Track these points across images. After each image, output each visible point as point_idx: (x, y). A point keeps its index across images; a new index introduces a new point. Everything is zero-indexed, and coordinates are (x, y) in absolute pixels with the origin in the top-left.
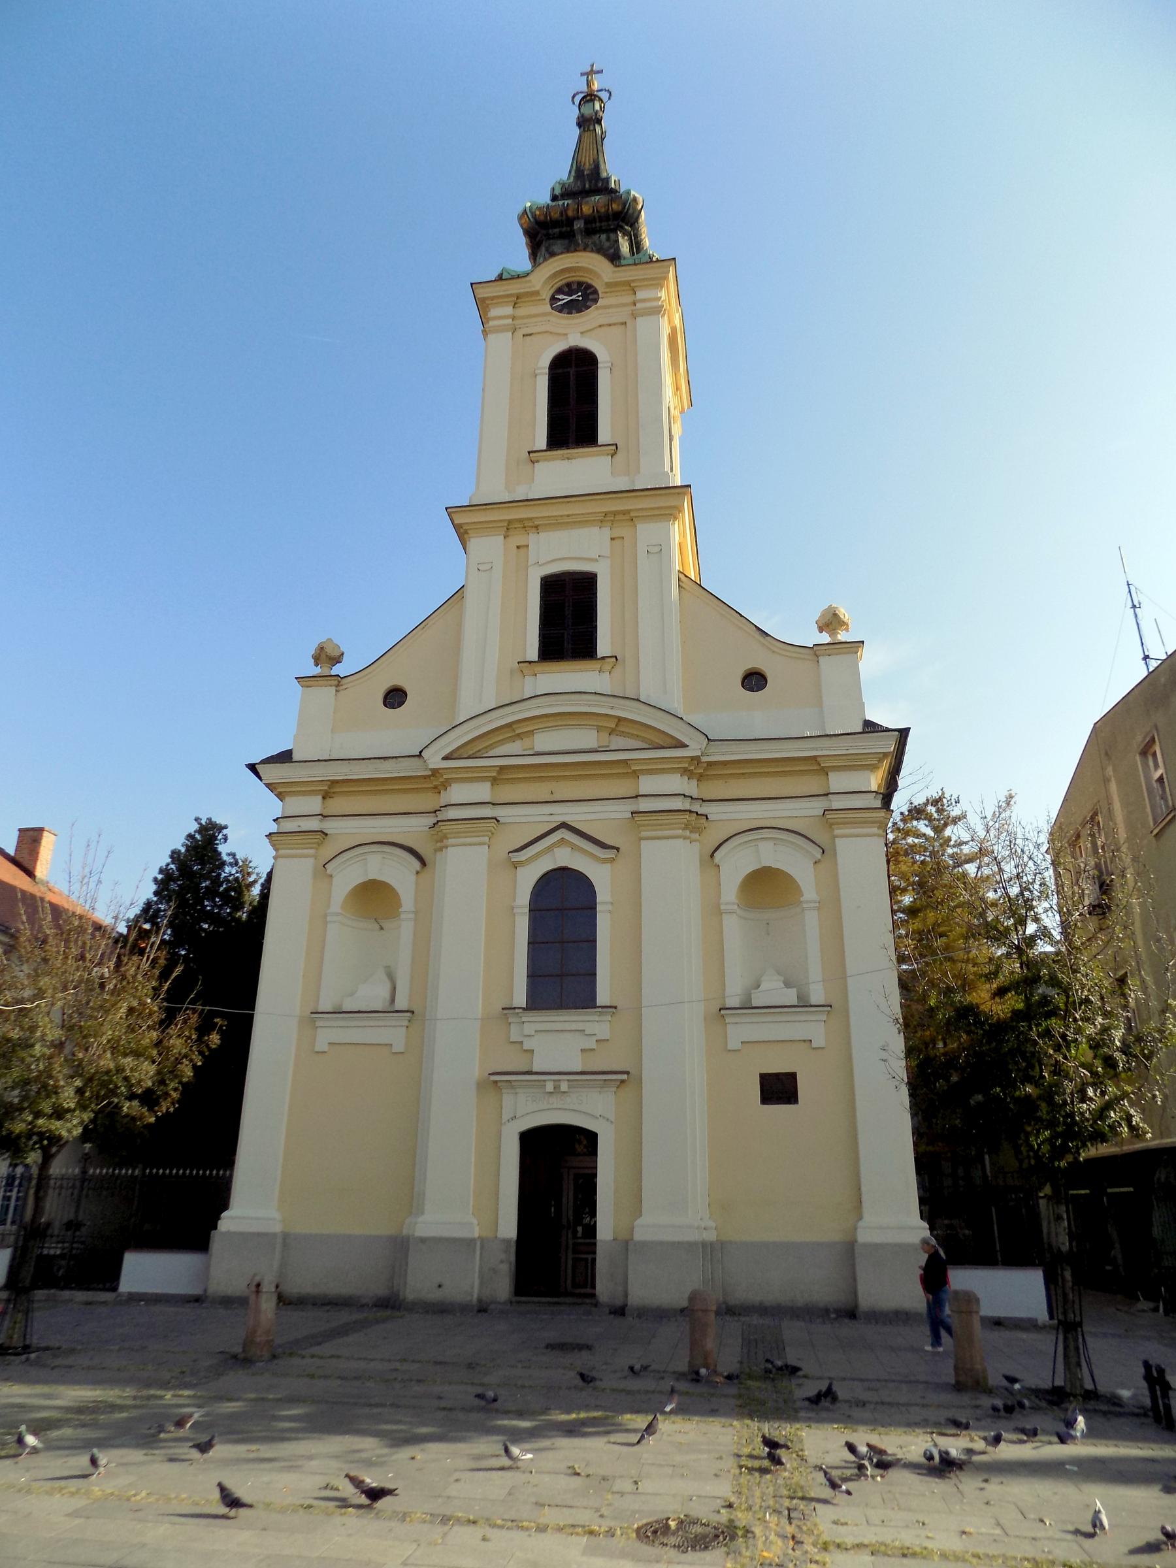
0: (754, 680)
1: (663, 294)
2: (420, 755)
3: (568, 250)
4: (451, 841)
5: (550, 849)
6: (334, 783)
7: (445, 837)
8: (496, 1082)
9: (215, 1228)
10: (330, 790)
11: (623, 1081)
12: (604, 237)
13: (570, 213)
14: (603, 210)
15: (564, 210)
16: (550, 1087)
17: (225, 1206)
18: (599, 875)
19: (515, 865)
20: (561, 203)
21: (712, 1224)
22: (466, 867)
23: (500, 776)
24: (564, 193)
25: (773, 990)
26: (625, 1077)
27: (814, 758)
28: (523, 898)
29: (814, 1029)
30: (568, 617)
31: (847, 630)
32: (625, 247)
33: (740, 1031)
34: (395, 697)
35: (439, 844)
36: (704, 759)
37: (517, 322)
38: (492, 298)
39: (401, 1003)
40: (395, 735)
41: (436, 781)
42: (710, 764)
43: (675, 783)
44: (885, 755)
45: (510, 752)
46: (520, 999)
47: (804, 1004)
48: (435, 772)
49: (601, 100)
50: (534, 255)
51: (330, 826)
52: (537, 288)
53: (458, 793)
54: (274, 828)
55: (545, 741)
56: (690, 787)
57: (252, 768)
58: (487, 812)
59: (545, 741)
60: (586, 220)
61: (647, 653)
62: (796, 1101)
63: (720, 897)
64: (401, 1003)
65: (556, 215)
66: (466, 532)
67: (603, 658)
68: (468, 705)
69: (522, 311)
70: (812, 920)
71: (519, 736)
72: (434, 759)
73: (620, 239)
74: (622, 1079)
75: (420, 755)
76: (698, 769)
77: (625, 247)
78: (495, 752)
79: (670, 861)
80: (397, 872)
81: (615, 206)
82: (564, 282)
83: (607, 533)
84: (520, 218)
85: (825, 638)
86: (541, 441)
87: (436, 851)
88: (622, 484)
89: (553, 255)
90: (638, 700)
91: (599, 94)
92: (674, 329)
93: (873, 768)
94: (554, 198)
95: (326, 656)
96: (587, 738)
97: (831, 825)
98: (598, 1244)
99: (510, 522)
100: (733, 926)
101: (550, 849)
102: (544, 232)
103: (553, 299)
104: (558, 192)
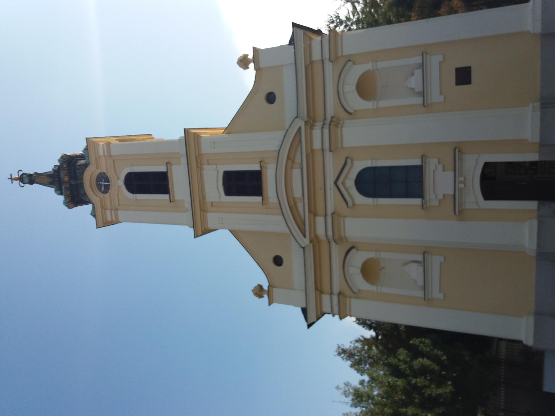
0: (271, 98)
1: (101, 143)
2: (304, 248)
3: (83, 187)
4: (342, 234)
5: (346, 189)
6: (316, 289)
7: (340, 237)
8: (459, 212)
9: (531, 348)
10: (319, 290)
11: (459, 151)
12: (78, 171)
13: (68, 186)
15: (67, 189)
16: (462, 186)
17: (520, 342)
18: (359, 165)
19: (354, 204)
21: (531, 105)
22: (355, 228)
23: (313, 213)
24: (60, 191)
25: (415, 82)
26: (457, 150)
27: (306, 67)
28: (369, 201)
29: (434, 61)
30: (243, 183)
31: (247, 55)
32: (82, 162)
33: (435, 97)
34: (278, 261)
35: (344, 240)
36: (306, 119)
39: (420, 258)
40: (295, 262)
41: (315, 241)
42: (308, 116)
43: (316, 133)
44: (304, 33)
45: (302, 208)
46: (417, 201)
47: (422, 66)
48: (311, 242)
49: (22, 174)
50: (86, 202)
51: (336, 290)
52: (98, 199)
53: (320, 231)
54: (337, 317)
55: (297, 192)
56: (319, 125)
57: (309, 326)
58: (329, 219)
59: (297, 192)
60: (70, 179)
61: (259, 150)
62: (469, 68)
63: (528, 33)
64: (420, 258)
65: (69, 192)
66: (205, 229)
67: (261, 167)
69: (109, 206)
70: (381, 65)
71: (295, 204)
72: (306, 242)
74: (458, 151)
75: (304, 248)
76: (310, 123)
77: (82, 162)
79: (353, 135)
80: (358, 259)
81: (65, 166)
83: (206, 167)
84: (70, 208)
85: (252, 66)
86: (165, 197)
88: (184, 160)
89: (85, 194)
90: (279, 150)
91: (20, 174)
92: (117, 140)
93: (311, 39)
94: (61, 194)
95: (259, 291)
96: (296, 174)
97: (337, 58)
98: (544, 158)
99: (201, 210)
100: (383, 104)
101: (346, 189)
102: (75, 198)
103: (103, 193)
104: (59, 192)
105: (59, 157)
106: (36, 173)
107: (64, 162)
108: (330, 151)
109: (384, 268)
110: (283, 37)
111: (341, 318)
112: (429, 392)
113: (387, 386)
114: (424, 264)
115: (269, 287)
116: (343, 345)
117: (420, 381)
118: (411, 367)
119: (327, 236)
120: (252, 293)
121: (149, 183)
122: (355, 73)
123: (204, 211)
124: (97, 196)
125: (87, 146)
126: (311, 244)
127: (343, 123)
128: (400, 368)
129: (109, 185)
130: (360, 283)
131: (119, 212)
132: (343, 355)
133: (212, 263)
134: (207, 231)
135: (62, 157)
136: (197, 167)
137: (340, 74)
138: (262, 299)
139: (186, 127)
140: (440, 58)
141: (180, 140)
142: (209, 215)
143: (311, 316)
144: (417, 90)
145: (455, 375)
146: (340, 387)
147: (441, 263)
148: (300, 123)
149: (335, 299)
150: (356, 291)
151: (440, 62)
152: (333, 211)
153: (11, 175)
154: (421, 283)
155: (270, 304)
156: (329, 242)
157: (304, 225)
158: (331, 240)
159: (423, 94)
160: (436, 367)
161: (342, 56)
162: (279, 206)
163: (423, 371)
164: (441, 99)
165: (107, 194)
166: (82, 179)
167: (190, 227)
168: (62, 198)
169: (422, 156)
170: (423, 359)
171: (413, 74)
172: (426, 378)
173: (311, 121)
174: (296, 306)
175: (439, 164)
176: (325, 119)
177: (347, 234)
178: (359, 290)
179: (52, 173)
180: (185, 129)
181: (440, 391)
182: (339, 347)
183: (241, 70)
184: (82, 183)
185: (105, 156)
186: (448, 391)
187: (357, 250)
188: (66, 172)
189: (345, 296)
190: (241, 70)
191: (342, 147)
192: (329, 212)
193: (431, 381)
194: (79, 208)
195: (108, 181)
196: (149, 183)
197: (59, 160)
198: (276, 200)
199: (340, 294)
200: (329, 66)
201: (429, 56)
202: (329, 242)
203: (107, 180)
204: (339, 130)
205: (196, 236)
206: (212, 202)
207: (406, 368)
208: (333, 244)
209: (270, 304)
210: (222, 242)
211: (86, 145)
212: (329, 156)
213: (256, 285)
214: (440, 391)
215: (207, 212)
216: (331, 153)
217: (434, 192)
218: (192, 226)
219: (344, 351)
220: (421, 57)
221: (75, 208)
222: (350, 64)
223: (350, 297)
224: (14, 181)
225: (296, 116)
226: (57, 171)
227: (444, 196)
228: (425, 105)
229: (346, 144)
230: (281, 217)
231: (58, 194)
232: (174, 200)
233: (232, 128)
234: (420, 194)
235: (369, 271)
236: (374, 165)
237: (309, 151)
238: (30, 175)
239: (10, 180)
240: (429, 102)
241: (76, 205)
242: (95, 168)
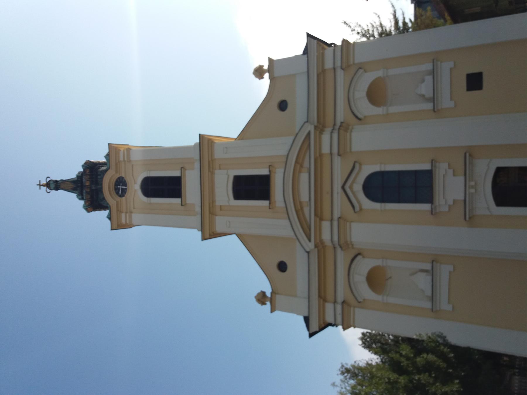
0: (283, 106)
1: (122, 150)
2: (308, 252)
3: (102, 192)
4: (348, 239)
5: (354, 193)
6: (320, 296)
8: (470, 218)
10: (322, 298)
11: (470, 155)
12: (99, 177)
15: (87, 193)
16: (473, 191)
19: (361, 209)
22: (361, 234)
23: (319, 217)
24: (81, 197)
25: (426, 89)
26: (468, 155)
28: (377, 206)
29: (446, 67)
30: (252, 188)
31: (263, 66)
32: (104, 168)
33: (446, 102)
34: (282, 267)
35: (350, 246)
36: (316, 124)
38: (117, 223)
39: (428, 266)
41: (320, 246)
42: (318, 121)
43: (326, 138)
44: (317, 43)
45: (309, 212)
46: (427, 207)
47: (433, 73)
48: (316, 246)
49: (50, 181)
51: (340, 299)
52: (115, 202)
53: (326, 236)
55: (304, 196)
56: (328, 130)
57: (311, 335)
58: (335, 223)
59: (304, 196)
60: (93, 185)
61: (270, 155)
64: (428, 266)
65: (89, 197)
66: (213, 233)
67: (270, 171)
68: (288, 232)
70: (391, 72)
71: (302, 208)
72: (310, 246)
74: (469, 155)
75: (308, 252)
76: (320, 128)
77: (104, 168)
78: (308, 220)
79: (362, 140)
80: (364, 266)
81: (88, 172)
83: (217, 172)
84: (89, 211)
85: (267, 75)
86: (177, 201)
87: (353, 248)
88: (197, 165)
89: (104, 198)
94: (82, 199)
95: (262, 298)
96: (304, 177)
97: (349, 66)
99: (210, 213)
100: (393, 109)
101: (354, 193)
102: (95, 203)
105: (83, 163)
108: (339, 155)
109: (390, 278)
110: (297, 48)
111: (344, 329)
112: (433, 390)
113: (386, 383)
114: (432, 272)
115: (272, 293)
116: (347, 364)
117: (424, 378)
118: (414, 364)
119: (332, 241)
120: (255, 300)
121: (163, 187)
122: (365, 80)
124: (112, 198)
125: (109, 152)
126: (316, 249)
127: (353, 128)
128: (402, 364)
129: (126, 189)
130: (365, 292)
131: (133, 215)
132: (346, 374)
133: (218, 267)
134: (214, 235)
135: (86, 163)
136: (209, 171)
137: (351, 81)
138: (264, 306)
139: (203, 133)
140: (451, 64)
141: (195, 145)
143: (315, 326)
144: (427, 96)
145: (463, 374)
146: (336, 384)
147: (450, 272)
148: (310, 128)
149: (339, 307)
150: (360, 300)
151: (451, 69)
152: (339, 216)
153: (40, 181)
154: (430, 294)
155: (272, 311)
156: (335, 248)
157: (310, 230)
158: (337, 246)
159: (433, 100)
160: (443, 365)
161: (354, 64)
162: (285, 209)
163: (428, 368)
164: (452, 104)
165: (124, 198)
166: (102, 184)
168: (82, 202)
169: (432, 160)
170: (428, 354)
171: (423, 81)
172: (430, 375)
173: (321, 126)
174: (298, 314)
175: (449, 168)
176: (335, 125)
177: (353, 239)
178: (364, 300)
179: (76, 179)
180: (200, 135)
181: (446, 389)
182: (343, 366)
183: (257, 80)
184: (102, 188)
185: (124, 161)
186: (455, 389)
187: (364, 257)
188: (88, 177)
189: (349, 305)
190: (257, 79)
191: (351, 152)
192: (336, 216)
193: (436, 379)
195: (126, 185)
196: (163, 187)
197: (83, 166)
198: (283, 205)
199: (344, 302)
200: (340, 74)
201: (439, 63)
202: (335, 248)
203: (125, 184)
204: (348, 134)
205: (204, 239)
206: (221, 206)
207: (408, 365)
208: (339, 250)
209: (272, 311)
210: (230, 249)
211: (108, 151)
212: (337, 160)
213: (259, 291)
214: (446, 389)
215: (216, 215)
216: (339, 157)
217: (444, 198)
218: (200, 228)
219: (348, 371)
220: (432, 64)
221: (93, 212)
222: (361, 71)
223: (354, 307)
224: (42, 187)
225: (306, 120)
226: (80, 177)
227: (454, 201)
228: (436, 110)
229: (355, 148)
230: (288, 221)
231: (80, 199)
232: (186, 204)
233: (244, 134)
234: (428, 198)
235: (375, 280)
236: (383, 170)
237: (318, 155)
238: (56, 182)
239: (38, 186)
240: (440, 108)
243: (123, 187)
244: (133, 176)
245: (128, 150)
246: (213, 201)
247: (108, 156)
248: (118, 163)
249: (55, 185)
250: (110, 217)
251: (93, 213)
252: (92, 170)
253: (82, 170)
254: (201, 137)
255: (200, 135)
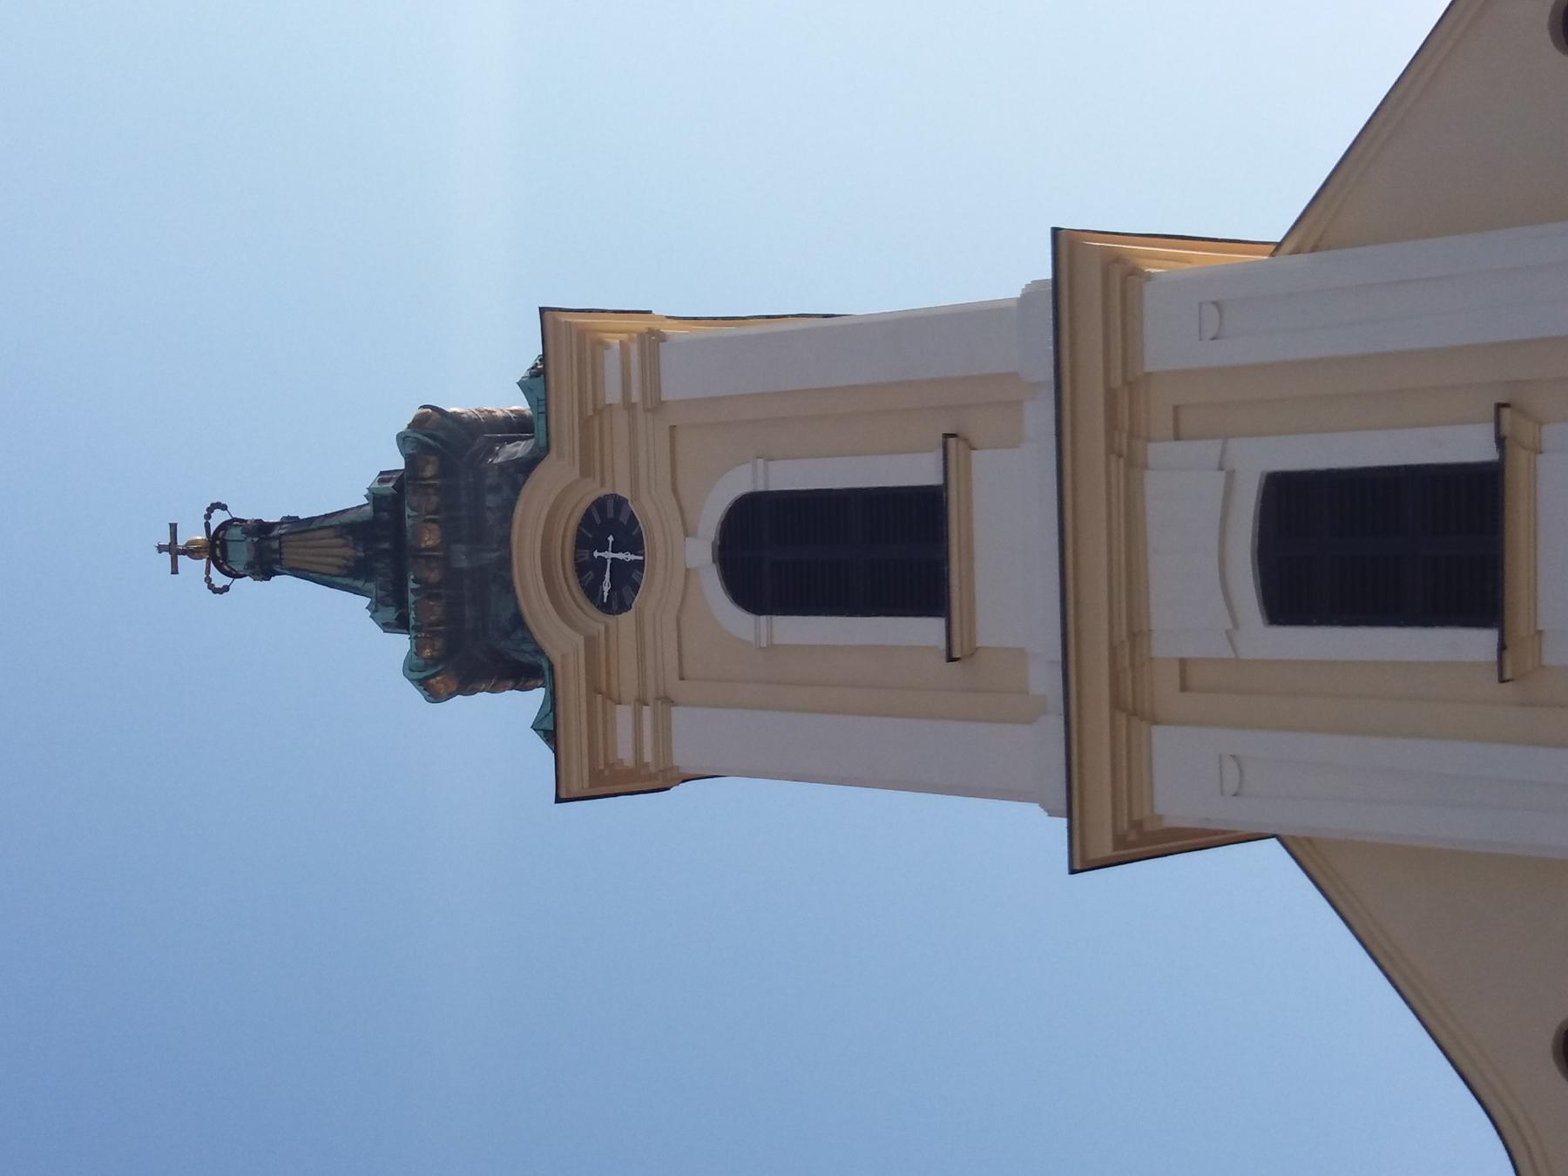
1: (615, 341)
3: (509, 587)
12: (491, 500)
14: (435, 499)
20: (411, 598)
30: (1377, 547)
32: (519, 449)
37: (651, 694)
49: (224, 526)
52: (580, 640)
60: (458, 551)
65: (436, 610)
66: (1137, 825)
67: (1500, 441)
73: (499, 460)
77: (519, 449)
81: (429, 471)
82: (573, 581)
83: (1161, 452)
84: (434, 696)
86: (924, 631)
88: (1039, 416)
89: (518, 621)
91: (215, 522)
94: (400, 624)
99: (1116, 704)
102: (467, 647)
103: (606, 608)
106: (292, 521)
107: (425, 449)
121: (856, 553)
123: (1134, 713)
125: (543, 359)
129: (640, 565)
131: (678, 715)
135: (418, 423)
136: (1111, 449)
142: (1162, 737)
153: (173, 527)
165: (626, 618)
166: (506, 541)
167: (1052, 813)
180: (1056, 232)
184: (506, 563)
185: (629, 406)
194: (482, 701)
195: (636, 545)
196: (856, 553)
197: (402, 439)
203: (631, 537)
205: (1081, 863)
206: (1183, 663)
210: (1246, 924)
224: (183, 560)
226: (391, 498)
231: (387, 627)
232: (974, 652)
233: (1322, 222)
238: (261, 529)
239: (167, 556)
241: (467, 686)
242: (575, 473)
243: (620, 556)
244: (675, 490)
245: (651, 339)
246: (1137, 635)
247: (537, 380)
248: (593, 418)
249: (250, 549)
250: (549, 729)
251: (460, 704)
252: (445, 449)
253: (399, 463)
254: (1065, 245)
255: (1056, 232)
